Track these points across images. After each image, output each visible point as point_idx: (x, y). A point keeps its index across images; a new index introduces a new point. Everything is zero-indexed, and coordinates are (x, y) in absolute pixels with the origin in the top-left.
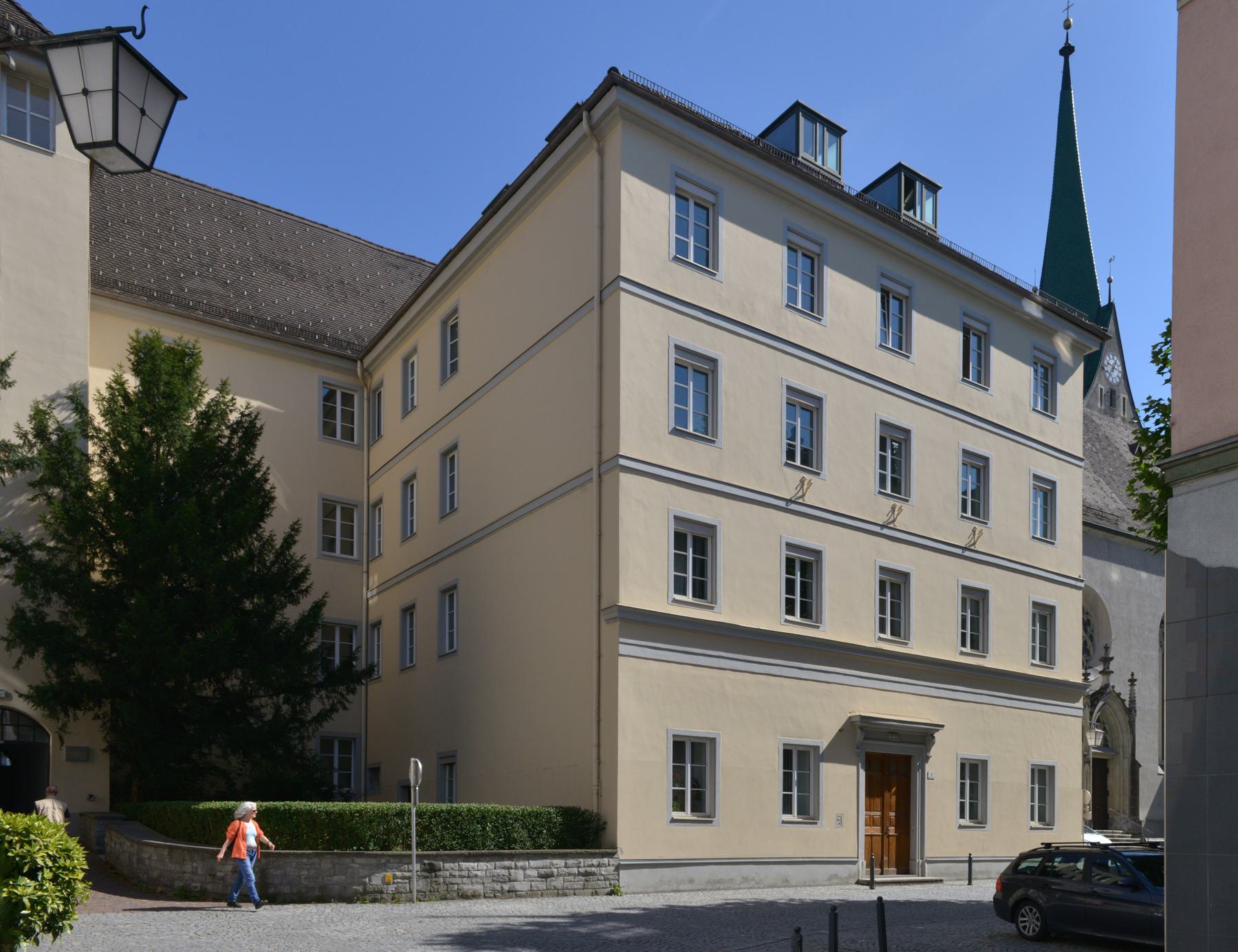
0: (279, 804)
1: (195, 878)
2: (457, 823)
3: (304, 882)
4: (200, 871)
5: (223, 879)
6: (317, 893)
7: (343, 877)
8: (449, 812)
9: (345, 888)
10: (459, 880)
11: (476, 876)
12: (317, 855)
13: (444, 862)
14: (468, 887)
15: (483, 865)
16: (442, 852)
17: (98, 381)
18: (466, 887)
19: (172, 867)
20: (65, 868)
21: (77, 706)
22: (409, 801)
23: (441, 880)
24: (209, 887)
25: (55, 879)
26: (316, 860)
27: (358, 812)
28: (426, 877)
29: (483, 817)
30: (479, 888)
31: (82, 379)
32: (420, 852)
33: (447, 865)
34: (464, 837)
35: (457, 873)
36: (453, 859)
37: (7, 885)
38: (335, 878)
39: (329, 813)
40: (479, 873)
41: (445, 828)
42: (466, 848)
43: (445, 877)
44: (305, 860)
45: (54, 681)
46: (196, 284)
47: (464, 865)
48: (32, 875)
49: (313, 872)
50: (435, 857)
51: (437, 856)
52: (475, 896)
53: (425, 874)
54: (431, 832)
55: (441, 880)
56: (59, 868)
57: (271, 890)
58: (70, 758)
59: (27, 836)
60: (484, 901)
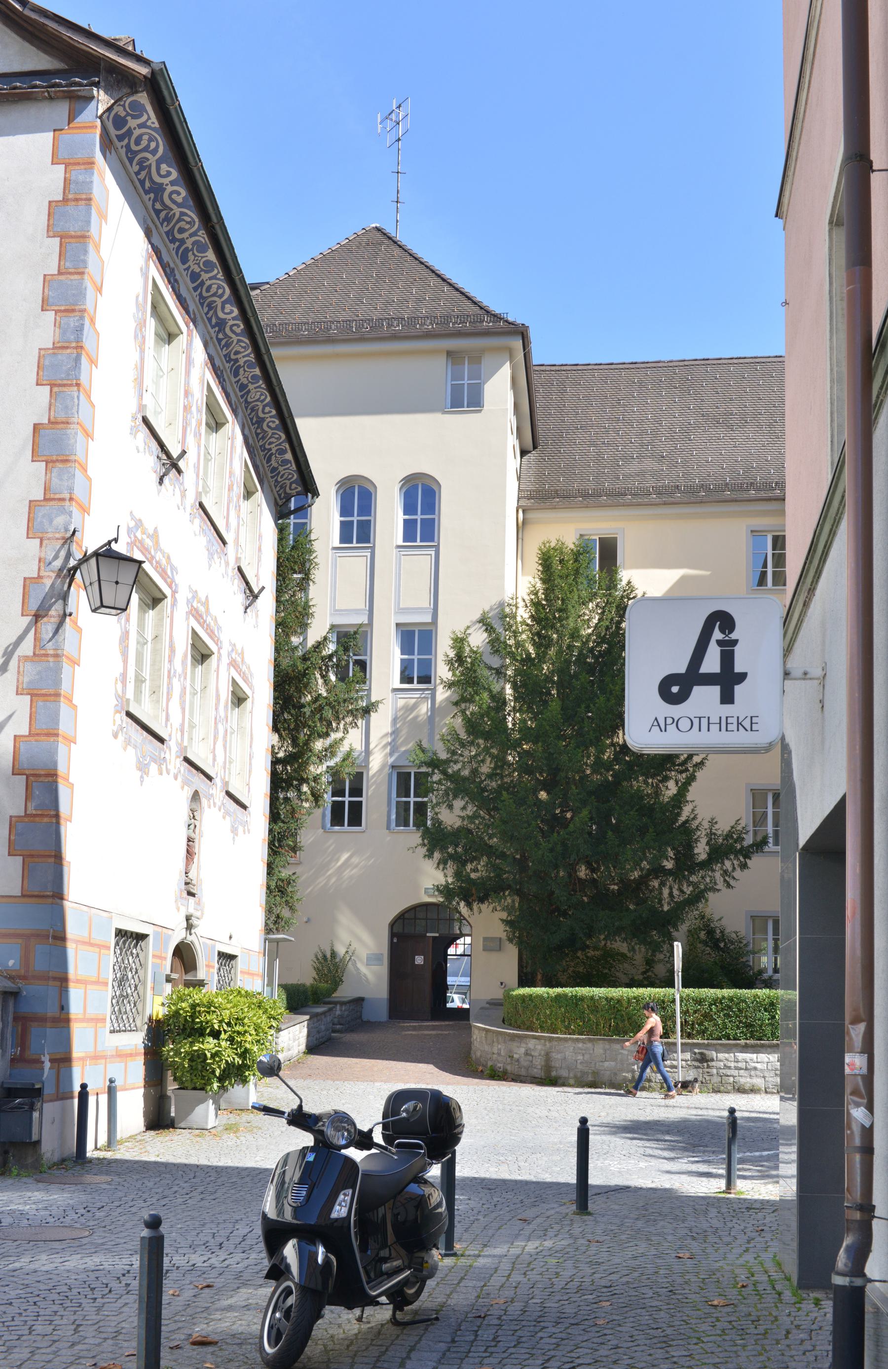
0: (568, 990)
1: (500, 1059)
2: (739, 1010)
3: (579, 1066)
4: (503, 1053)
5: (518, 1060)
6: (590, 1078)
7: (613, 1063)
8: (731, 999)
9: (615, 1074)
10: (735, 1073)
11: (755, 1069)
12: (583, 1041)
13: (717, 1051)
14: (745, 1080)
15: (763, 1057)
16: (724, 1041)
17: (524, 592)
18: (742, 1080)
19: (487, 1048)
20: (239, 1033)
21: (481, 900)
22: (673, 987)
23: (715, 1071)
24: (509, 1068)
25: (231, 1040)
26: (589, 1045)
27: (635, 998)
28: (697, 1067)
29: (772, 1004)
30: (759, 1082)
31: (494, 600)
32: (684, 1041)
33: (721, 1056)
34: (748, 1026)
35: (732, 1065)
36: (728, 1049)
37: (199, 1042)
38: (606, 1064)
39: (608, 1000)
40: (759, 1066)
41: (727, 1016)
42: (752, 1037)
43: (718, 1068)
44: (580, 1045)
45: (450, 880)
46: (634, 467)
47: (741, 1056)
48: (216, 1035)
49: (587, 1057)
50: (707, 1047)
51: (708, 1045)
52: (753, 1090)
53: (696, 1064)
54: (712, 1019)
55: (715, 1071)
56: (234, 1032)
57: (554, 1074)
58: (486, 949)
59: (209, 1008)
60: (763, 1095)
